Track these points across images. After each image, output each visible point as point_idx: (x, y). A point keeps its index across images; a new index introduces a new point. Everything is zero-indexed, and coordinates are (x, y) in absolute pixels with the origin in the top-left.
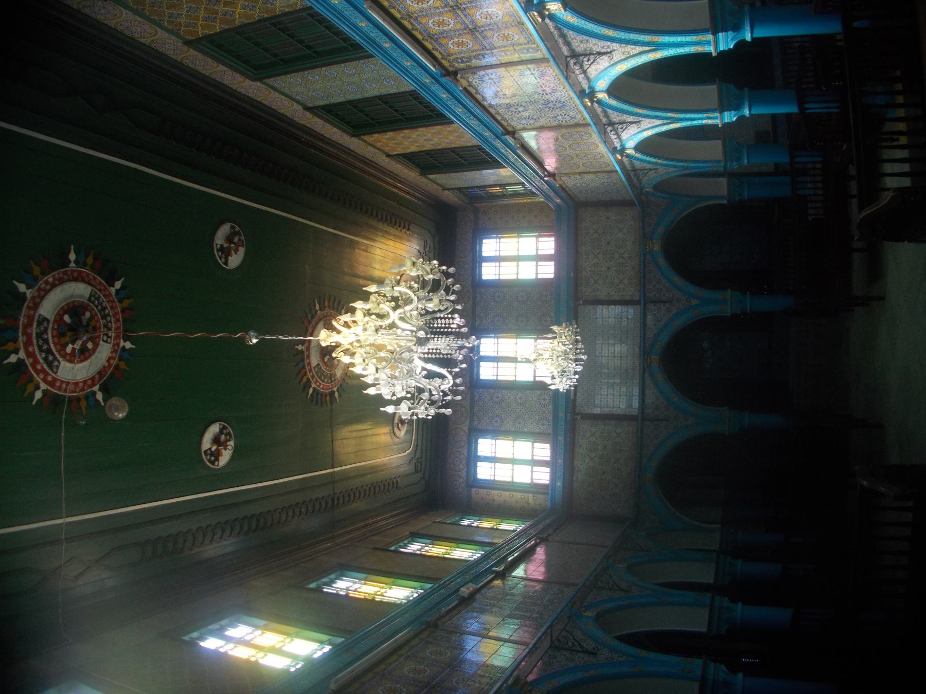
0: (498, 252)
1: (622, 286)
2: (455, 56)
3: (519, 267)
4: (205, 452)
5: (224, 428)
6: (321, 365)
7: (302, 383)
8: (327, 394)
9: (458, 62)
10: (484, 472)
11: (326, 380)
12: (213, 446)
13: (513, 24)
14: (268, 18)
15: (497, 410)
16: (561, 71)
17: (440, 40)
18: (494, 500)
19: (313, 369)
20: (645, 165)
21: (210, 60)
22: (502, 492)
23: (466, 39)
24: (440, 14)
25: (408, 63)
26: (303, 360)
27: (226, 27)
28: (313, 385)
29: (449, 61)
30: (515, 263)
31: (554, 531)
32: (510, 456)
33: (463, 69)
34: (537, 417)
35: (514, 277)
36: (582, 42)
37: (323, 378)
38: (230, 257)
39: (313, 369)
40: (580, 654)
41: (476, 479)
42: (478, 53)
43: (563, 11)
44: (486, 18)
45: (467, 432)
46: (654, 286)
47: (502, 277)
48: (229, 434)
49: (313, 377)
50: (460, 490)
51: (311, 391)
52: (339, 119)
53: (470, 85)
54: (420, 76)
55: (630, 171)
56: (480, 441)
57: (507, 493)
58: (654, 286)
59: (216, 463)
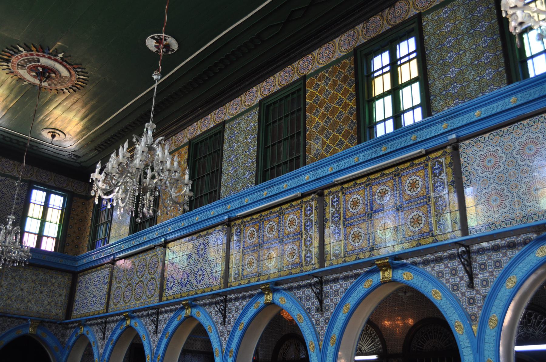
0: (52, 206)
2: (242, 229)
3: (37, 220)
6: (38, 64)
7: (32, 46)
9: (237, 229)
11: (22, 62)
13: (260, 270)
14: (306, 134)
19: (38, 57)
21: (286, 84)
23: (255, 240)
24: (279, 231)
25: (246, 200)
27: (307, 106)
28: (24, 52)
29: (239, 224)
30: (40, 217)
33: (230, 231)
36: (237, 308)
37: (26, 60)
38: (155, 41)
39: (38, 57)
42: (242, 243)
44: (268, 256)
49: (32, 55)
51: (21, 49)
52: (208, 138)
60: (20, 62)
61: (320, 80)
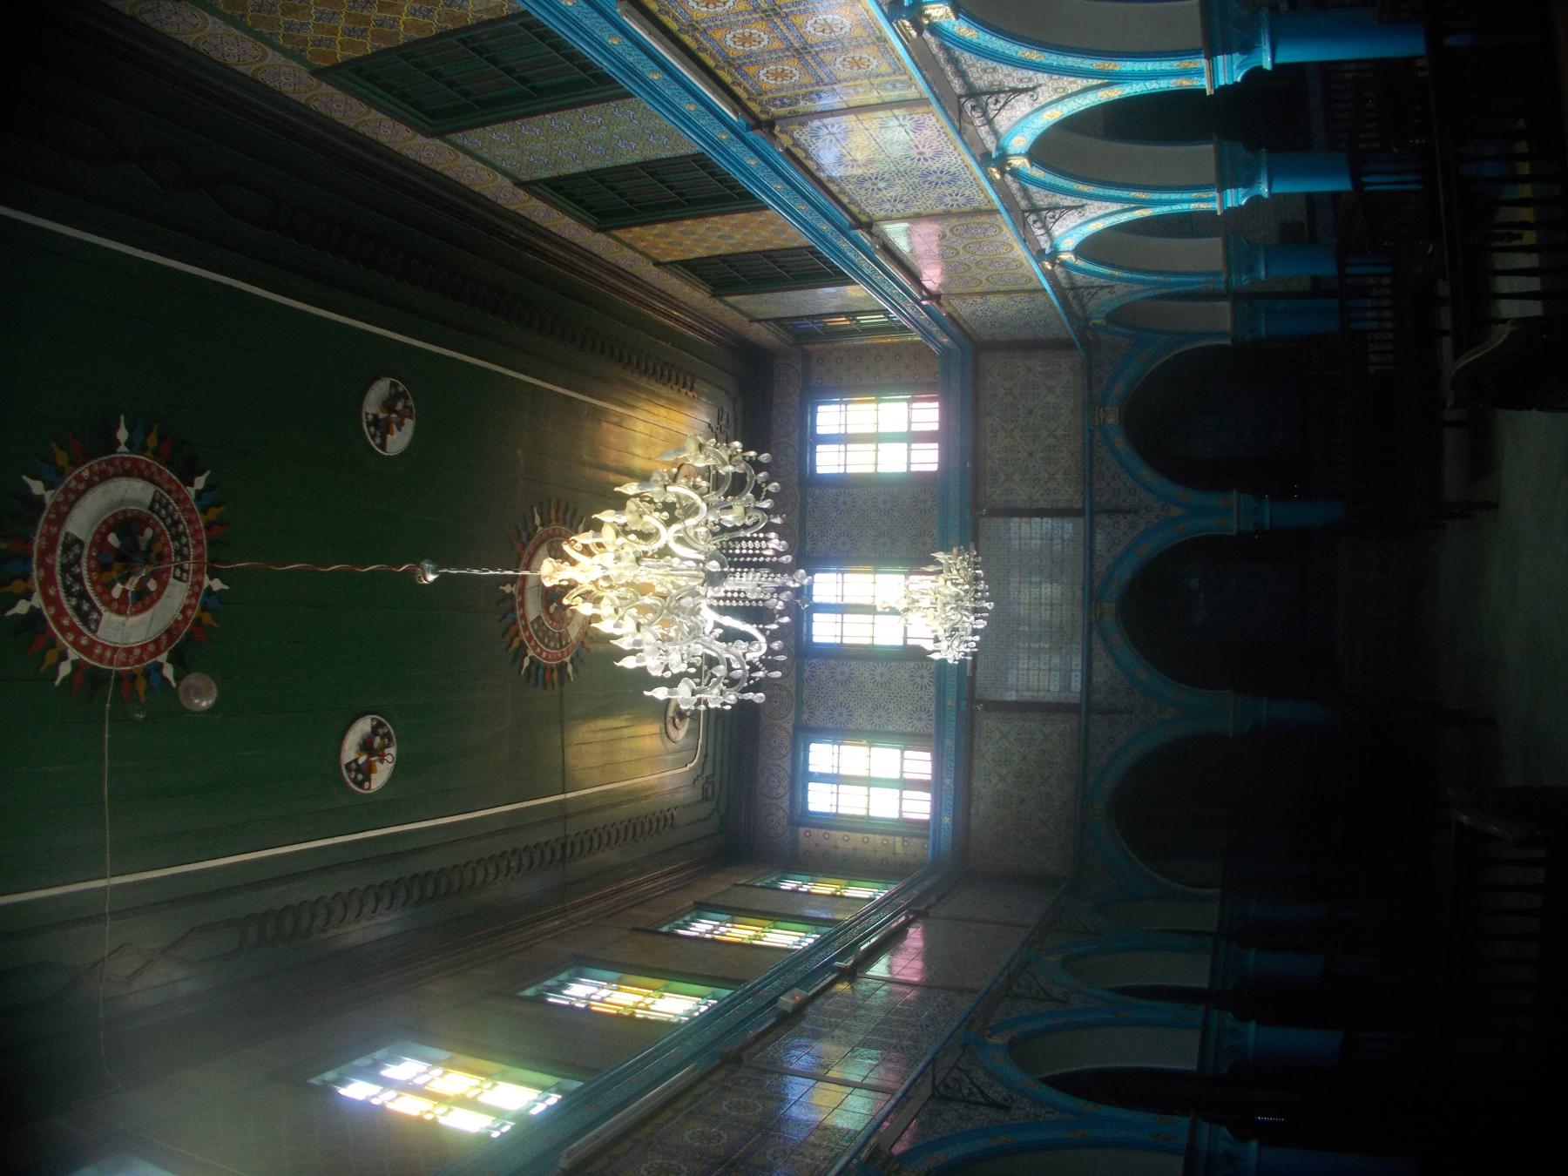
0: (843, 427)
1: (1052, 485)
2: (770, 95)
3: (879, 453)
4: (348, 766)
5: (380, 725)
6: (544, 618)
7: (511, 649)
8: (555, 667)
9: (775, 106)
10: (819, 799)
11: (552, 644)
12: (360, 756)
13: (869, 41)
14: (454, 30)
15: (841, 694)
16: (950, 119)
17: (744, 68)
18: (836, 847)
19: (530, 626)
20: (1093, 279)
21: (355, 102)
22: (850, 834)
23: (790, 66)
24: (745, 23)
25: (690, 107)
26: (513, 610)
27: (383, 46)
28: (531, 653)
29: (760, 104)
30: (872, 446)
31: (938, 900)
32: (864, 773)
33: (785, 117)
34: (910, 707)
35: (870, 469)
36: (985, 71)
37: (546, 640)
38: (389, 436)
39: (530, 626)
40: (981, 1109)
41: (806, 812)
42: (810, 89)
43: (954, 19)
45: (791, 731)
46: (1108, 484)
47: (850, 470)
48: (388, 735)
49: (530, 638)
50: (779, 830)
51: (526, 662)
53: (796, 143)
54: (710, 129)
55: (1066, 289)
56: (814, 747)
57: (859, 836)
58: (1108, 484)
59: (366, 785)
60: (554, 648)
61: (305, 41)
